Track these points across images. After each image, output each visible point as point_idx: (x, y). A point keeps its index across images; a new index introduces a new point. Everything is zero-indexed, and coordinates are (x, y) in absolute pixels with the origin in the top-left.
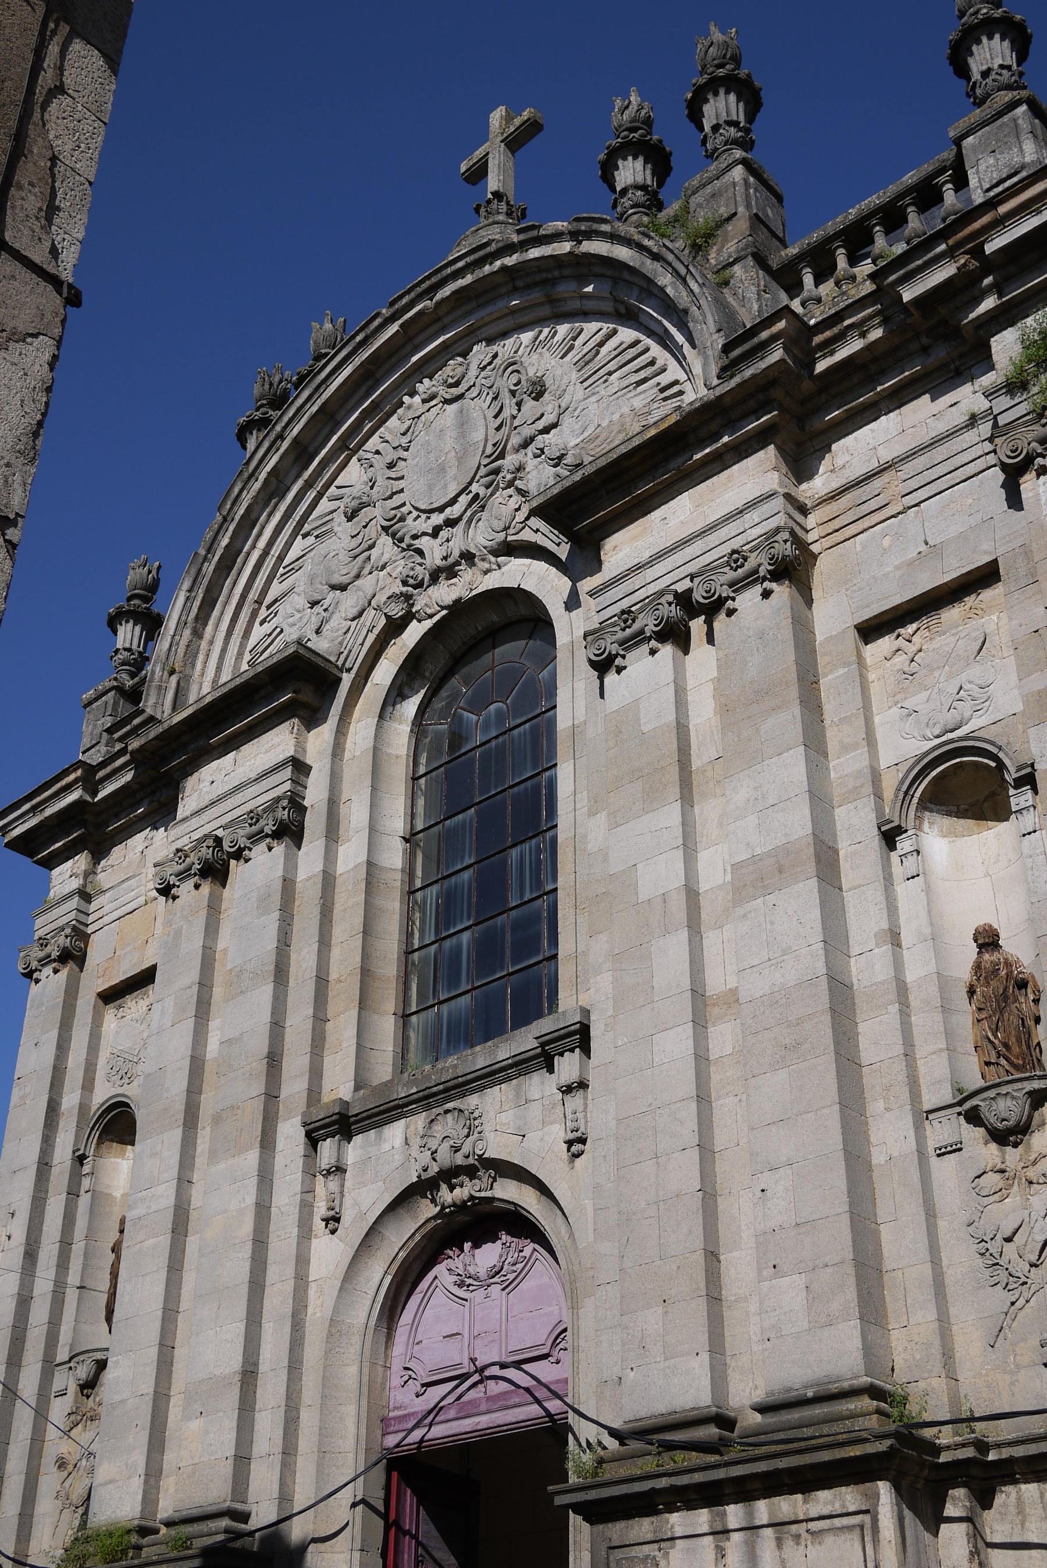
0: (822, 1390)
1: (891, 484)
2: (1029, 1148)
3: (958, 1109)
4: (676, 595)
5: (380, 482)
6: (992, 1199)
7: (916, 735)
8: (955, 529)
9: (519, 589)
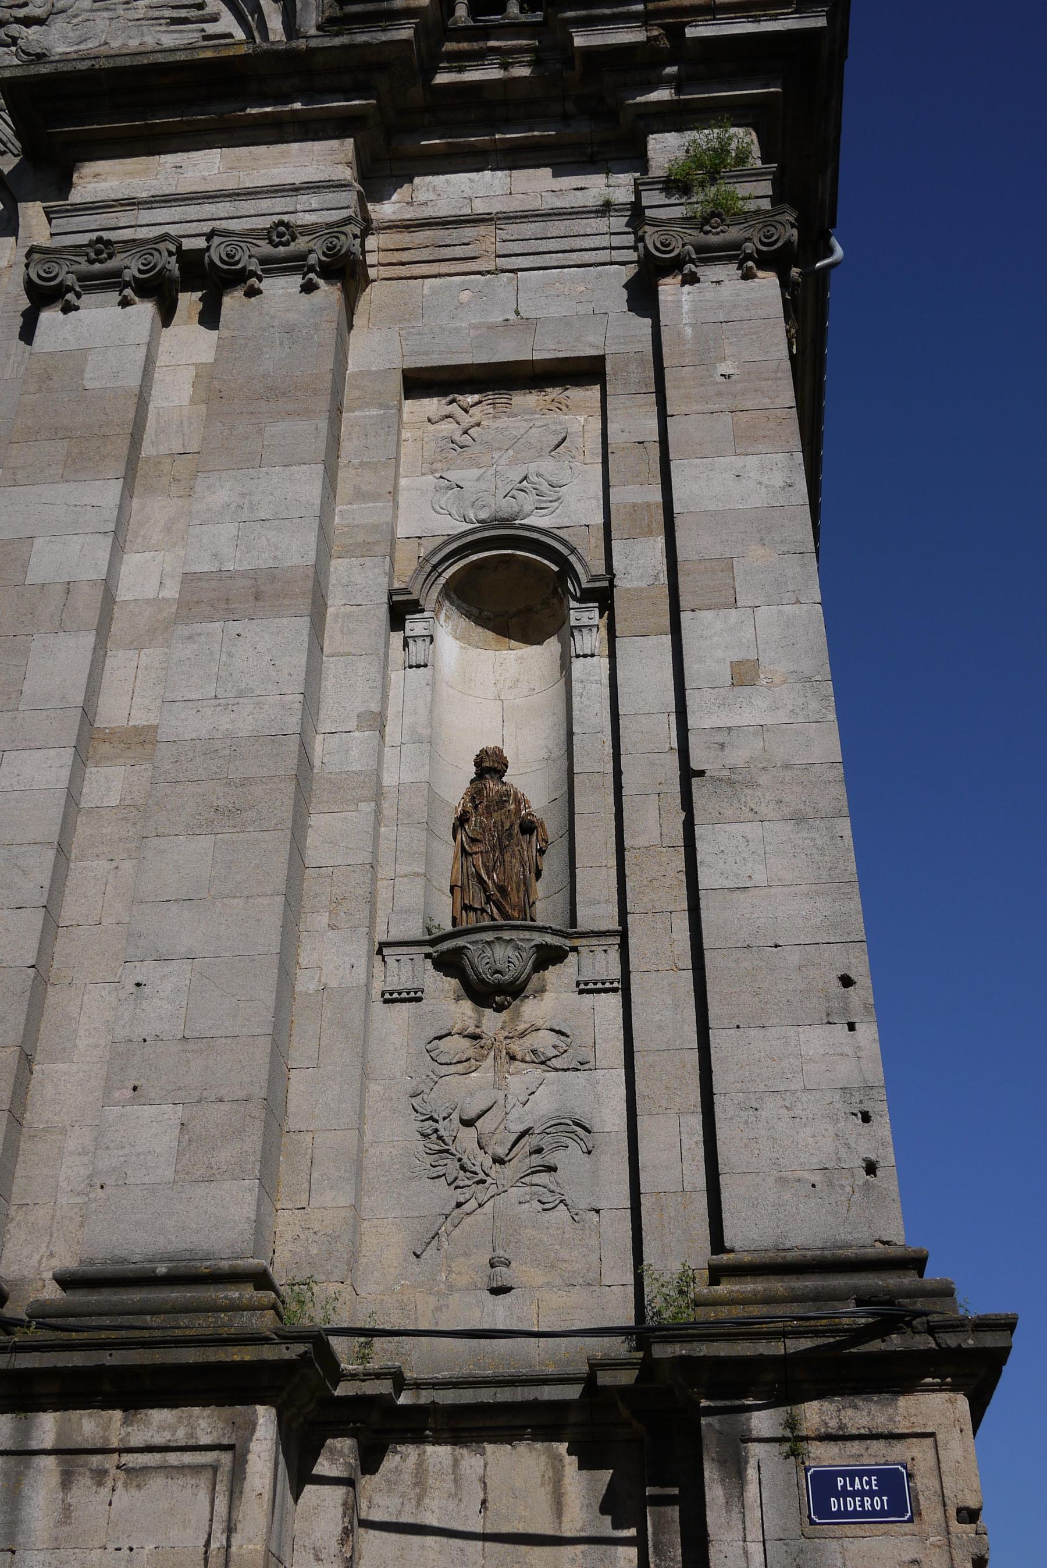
0: (182, 1267)
1: (484, 239)
2: (517, 1015)
3: (429, 950)
6: (453, 1069)
7: (454, 512)
8: (556, 310)
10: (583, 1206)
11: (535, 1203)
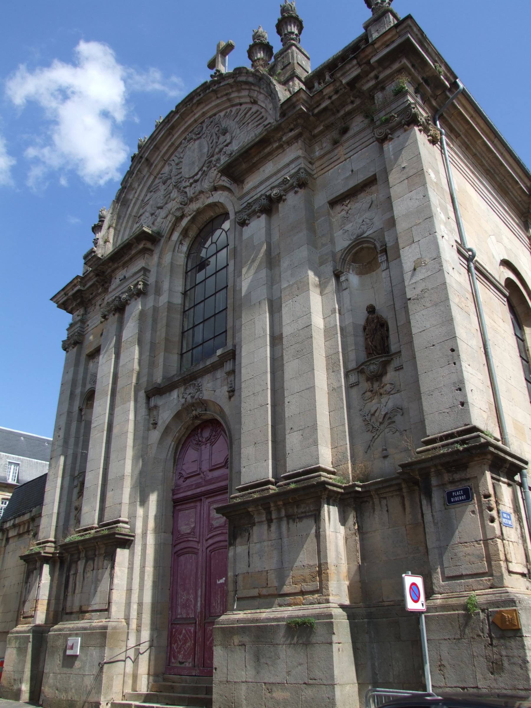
4: (266, 196)
5: (174, 170)
9: (219, 202)
10: (402, 430)
11: (391, 432)
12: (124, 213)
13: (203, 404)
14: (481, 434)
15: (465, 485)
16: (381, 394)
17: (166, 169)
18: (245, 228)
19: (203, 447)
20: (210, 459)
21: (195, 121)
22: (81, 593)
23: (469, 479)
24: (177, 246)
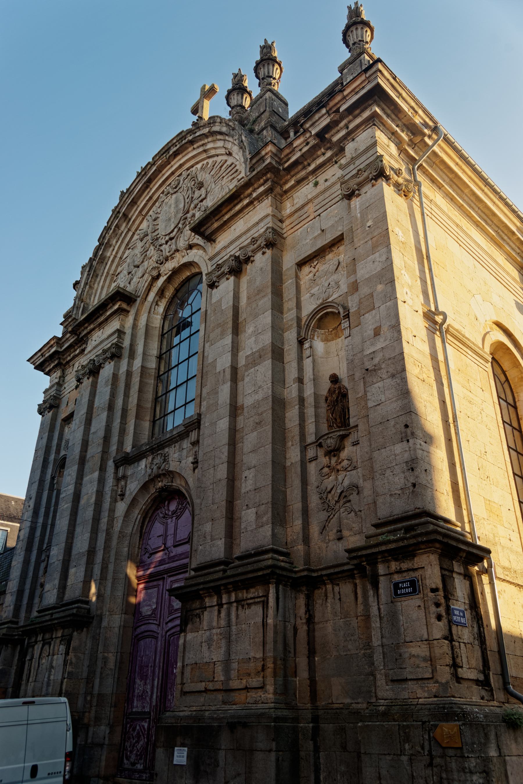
4: (235, 257)
9: (193, 262)
10: (357, 510)
11: (346, 513)
12: (102, 271)
13: (170, 474)
14: (430, 519)
15: (413, 575)
16: (338, 471)
17: (144, 225)
18: (215, 290)
19: (169, 521)
20: (175, 534)
21: (173, 173)
22: (35, 681)
23: (416, 569)
24: (153, 307)
